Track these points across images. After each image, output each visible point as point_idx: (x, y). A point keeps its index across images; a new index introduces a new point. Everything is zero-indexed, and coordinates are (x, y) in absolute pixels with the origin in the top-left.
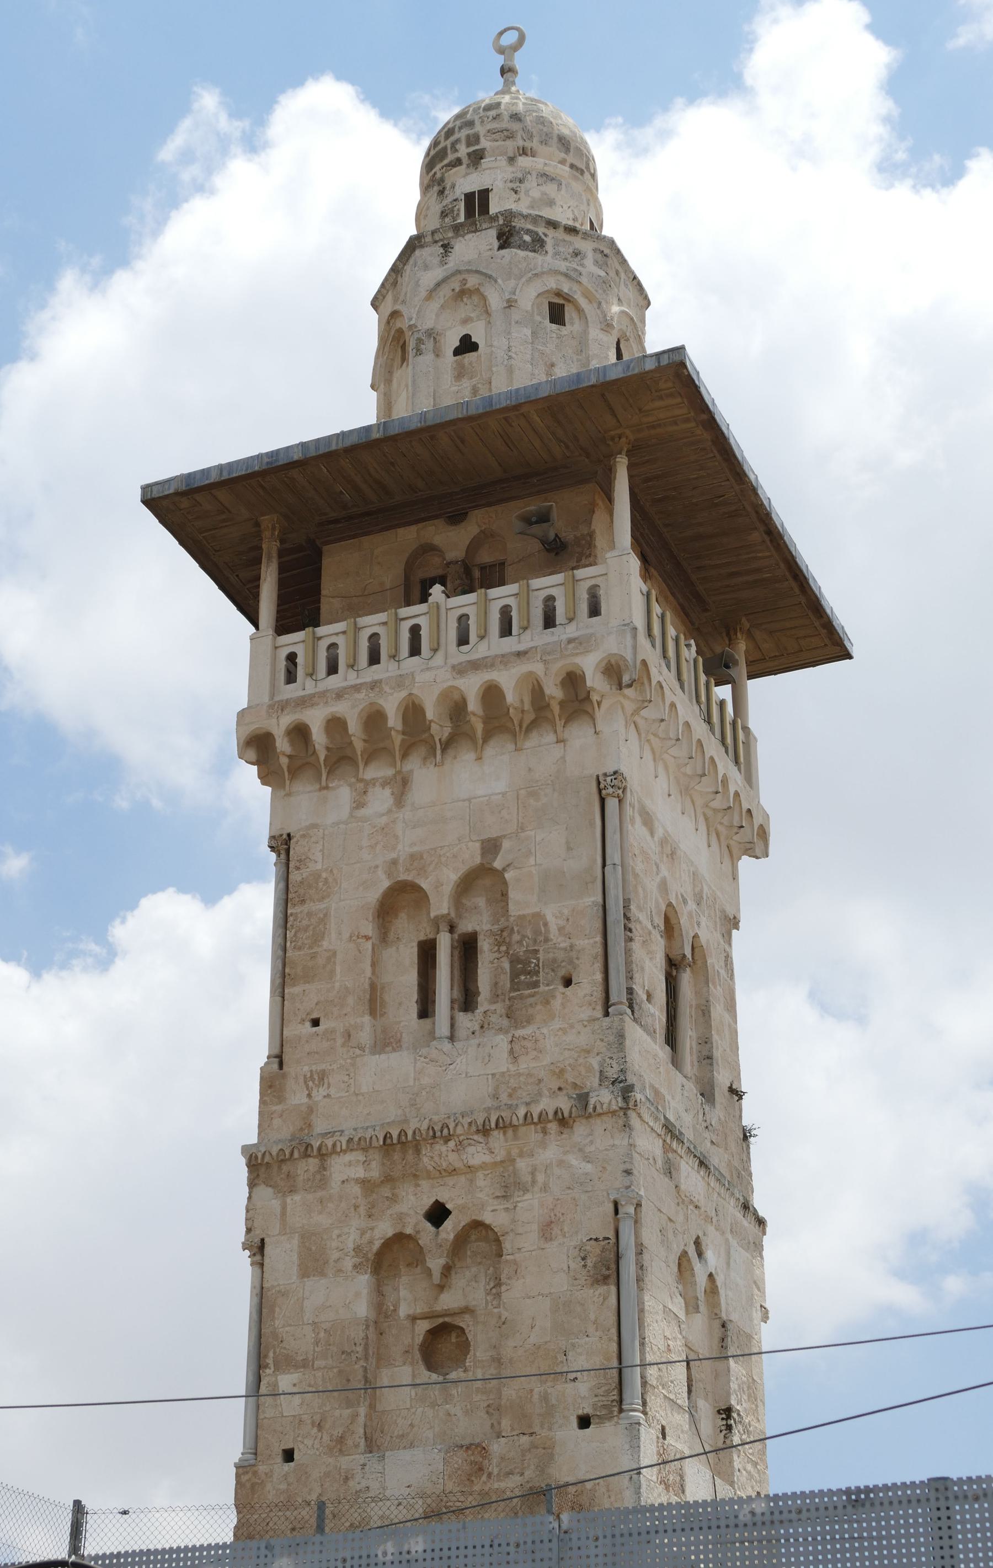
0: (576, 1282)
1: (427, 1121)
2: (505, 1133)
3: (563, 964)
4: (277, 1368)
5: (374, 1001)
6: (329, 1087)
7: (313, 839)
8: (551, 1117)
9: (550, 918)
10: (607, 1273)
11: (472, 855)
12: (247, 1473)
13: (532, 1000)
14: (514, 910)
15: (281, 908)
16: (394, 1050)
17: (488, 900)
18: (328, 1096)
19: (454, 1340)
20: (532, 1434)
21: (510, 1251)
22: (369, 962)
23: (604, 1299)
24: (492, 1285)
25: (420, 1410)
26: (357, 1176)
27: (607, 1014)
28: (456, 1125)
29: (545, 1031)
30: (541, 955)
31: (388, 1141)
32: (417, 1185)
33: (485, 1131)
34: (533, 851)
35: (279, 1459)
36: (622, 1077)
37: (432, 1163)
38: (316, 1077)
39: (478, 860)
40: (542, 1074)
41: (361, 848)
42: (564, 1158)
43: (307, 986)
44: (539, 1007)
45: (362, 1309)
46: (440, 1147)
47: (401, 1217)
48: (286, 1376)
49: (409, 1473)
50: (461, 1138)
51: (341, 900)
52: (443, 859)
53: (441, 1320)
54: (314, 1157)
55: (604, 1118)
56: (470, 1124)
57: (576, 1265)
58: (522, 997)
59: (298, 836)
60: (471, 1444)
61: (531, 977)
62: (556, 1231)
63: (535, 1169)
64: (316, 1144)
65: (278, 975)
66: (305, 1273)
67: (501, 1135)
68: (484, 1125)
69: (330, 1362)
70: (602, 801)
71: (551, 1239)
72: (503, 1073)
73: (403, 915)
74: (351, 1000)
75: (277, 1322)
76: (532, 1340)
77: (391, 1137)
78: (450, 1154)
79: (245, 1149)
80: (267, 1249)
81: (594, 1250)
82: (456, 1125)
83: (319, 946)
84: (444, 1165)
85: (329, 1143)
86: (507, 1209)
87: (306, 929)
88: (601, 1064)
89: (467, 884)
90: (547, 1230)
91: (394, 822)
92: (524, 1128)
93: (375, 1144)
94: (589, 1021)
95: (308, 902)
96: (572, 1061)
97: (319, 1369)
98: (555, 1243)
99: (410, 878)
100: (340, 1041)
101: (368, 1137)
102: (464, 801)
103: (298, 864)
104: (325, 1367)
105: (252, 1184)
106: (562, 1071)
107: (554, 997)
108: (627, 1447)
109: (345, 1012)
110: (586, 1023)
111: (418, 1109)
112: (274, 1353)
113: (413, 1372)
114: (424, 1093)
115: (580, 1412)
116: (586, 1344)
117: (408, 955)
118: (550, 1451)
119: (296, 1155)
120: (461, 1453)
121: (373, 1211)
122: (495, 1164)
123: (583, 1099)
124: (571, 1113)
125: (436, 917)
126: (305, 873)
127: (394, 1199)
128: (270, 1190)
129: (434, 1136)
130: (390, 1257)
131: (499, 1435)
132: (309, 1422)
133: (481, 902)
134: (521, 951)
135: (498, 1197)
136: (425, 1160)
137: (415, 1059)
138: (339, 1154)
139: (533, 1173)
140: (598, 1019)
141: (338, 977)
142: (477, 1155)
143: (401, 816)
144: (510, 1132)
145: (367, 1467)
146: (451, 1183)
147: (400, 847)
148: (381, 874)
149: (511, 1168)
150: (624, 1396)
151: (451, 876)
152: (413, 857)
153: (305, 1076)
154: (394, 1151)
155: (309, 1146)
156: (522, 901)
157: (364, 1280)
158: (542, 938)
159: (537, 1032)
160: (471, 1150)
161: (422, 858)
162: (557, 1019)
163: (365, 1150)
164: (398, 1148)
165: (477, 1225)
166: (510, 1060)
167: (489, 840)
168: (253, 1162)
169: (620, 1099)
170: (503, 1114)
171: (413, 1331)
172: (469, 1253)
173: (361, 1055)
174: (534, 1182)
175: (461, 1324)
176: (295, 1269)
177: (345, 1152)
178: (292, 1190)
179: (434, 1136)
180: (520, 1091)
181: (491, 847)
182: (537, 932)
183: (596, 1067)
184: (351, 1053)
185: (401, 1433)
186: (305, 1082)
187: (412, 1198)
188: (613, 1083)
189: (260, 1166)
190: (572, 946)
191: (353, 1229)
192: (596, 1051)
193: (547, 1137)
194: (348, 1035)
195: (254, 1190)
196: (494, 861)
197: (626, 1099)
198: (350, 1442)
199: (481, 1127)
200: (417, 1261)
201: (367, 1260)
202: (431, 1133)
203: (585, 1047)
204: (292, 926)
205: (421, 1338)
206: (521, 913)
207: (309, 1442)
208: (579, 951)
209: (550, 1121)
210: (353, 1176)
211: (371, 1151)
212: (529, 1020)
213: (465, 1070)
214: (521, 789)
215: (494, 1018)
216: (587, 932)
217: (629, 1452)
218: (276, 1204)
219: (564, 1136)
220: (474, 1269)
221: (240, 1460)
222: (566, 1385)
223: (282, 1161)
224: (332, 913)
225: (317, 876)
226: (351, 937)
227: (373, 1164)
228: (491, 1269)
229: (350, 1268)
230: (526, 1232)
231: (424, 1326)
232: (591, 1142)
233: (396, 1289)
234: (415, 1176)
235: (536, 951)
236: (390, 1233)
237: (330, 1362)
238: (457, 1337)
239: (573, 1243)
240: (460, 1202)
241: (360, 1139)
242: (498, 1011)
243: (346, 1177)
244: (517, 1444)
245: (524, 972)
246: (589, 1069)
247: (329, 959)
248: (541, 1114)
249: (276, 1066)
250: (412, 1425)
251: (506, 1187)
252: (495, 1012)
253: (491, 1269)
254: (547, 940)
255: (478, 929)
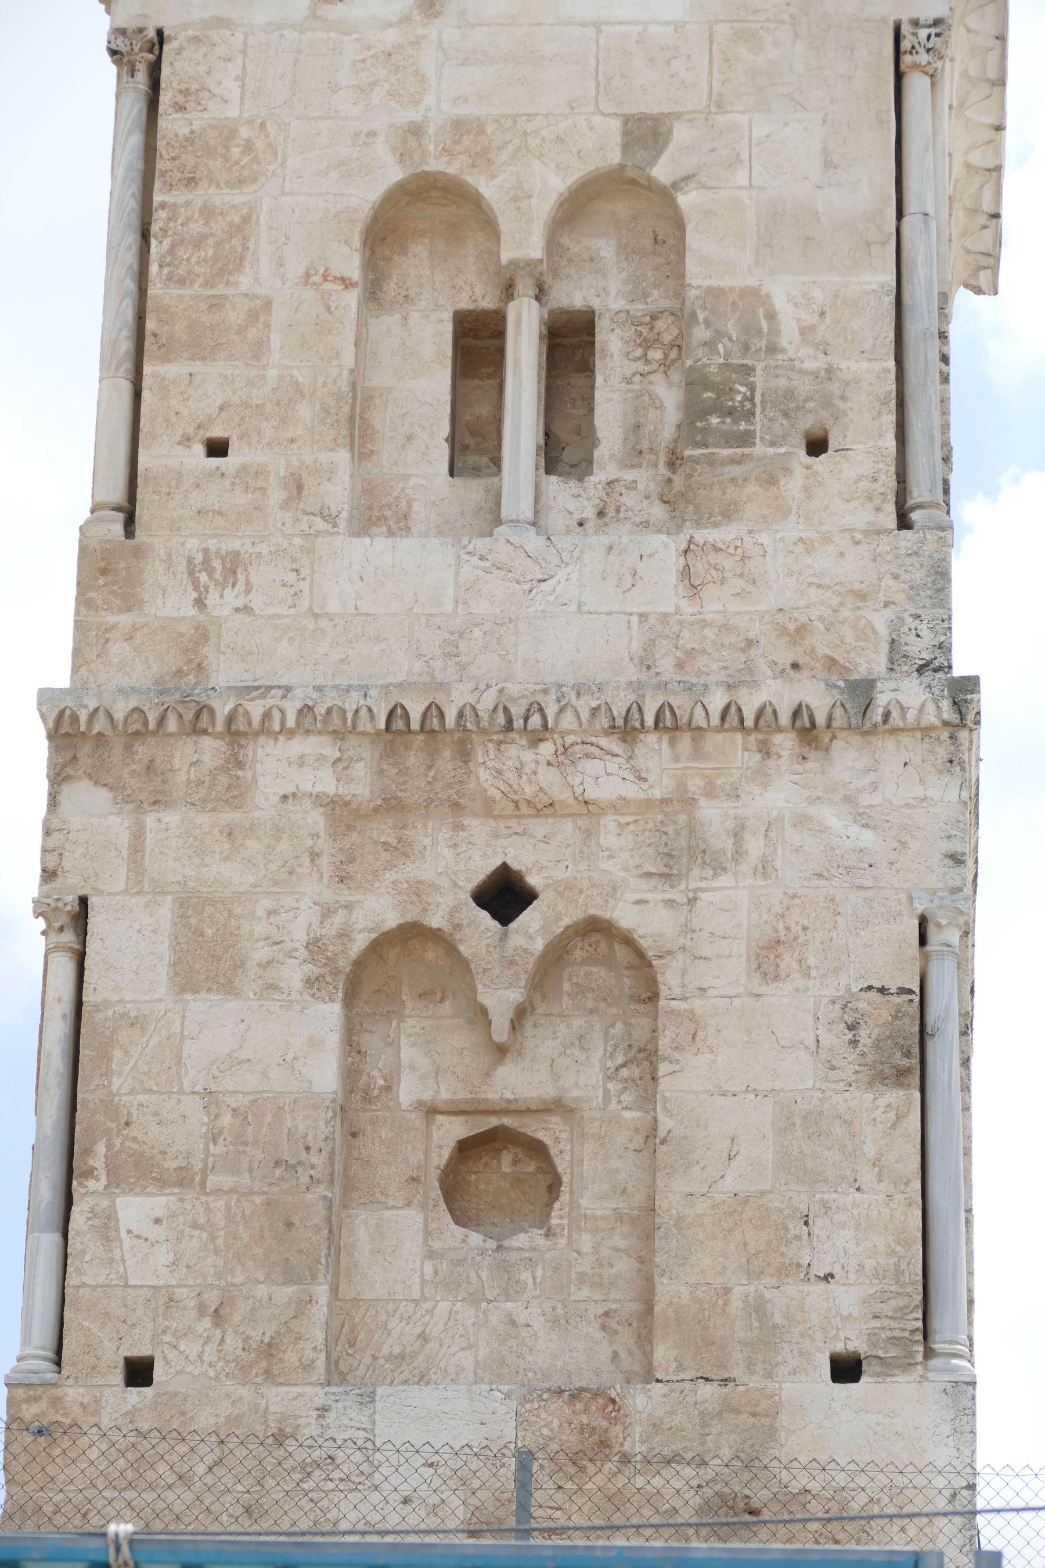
0: (832, 1074)
1: (493, 692)
2: (672, 742)
3: (810, 405)
4: (116, 1179)
5: (357, 422)
6: (248, 592)
7: (219, 51)
8: (785, 719)
9: (780, 303)
10: (906, 1062)
11: (602, 146)
12: (37, 1399)
13: (736, 470)
14: (697, 275)
15: (135, 188)
16: (391, 534)
17: (623, 250)
18: (246, 609)
19: (506, 1168)
20: (725, 1382)
21: (677, 992)
22: (351, 336)
23: (898, 1118)
24: (620, 1059)
25: (443, 1306)
26: (319, 788)
27: (904, 522)
28: (561, 710)
29: (764, 538)
30: (758, 379)
31: (399, 724)
32: (458, 827)
33: (627, 730)
34: (745, 155)
35: (118, 1376)
36: (941, 660)
37: (501, 785)
38: (217, 564)
39: (615, 157)
40: (756, 630)
41: (335, 89)
42: (812, 810)
43: (198, 367)
44: (753, 488)
45: (325, 1075)
46: (518, 752)
47: (418, 890)
48: (138, 1200)
49: (430, 1437)
50: (570, 739)
51: (283, 193)
52: (533, 142)
53: (493, 1122)
54: (217, 736)
55: (905, 739)
56: (595, 711)
57: (834, 1038)
58: (712, 462)
59: (182, 37)
60: (581, 1390)
61: (736, 422)
62: (788, 961)
63: (743, 827)
64: (223, 708)
65: (126, 333)
66: (186, 981)
67: (665, 745)
68: (626, 719)
69: (246, 1180)
70: (899, 76)
71: (777, 978)
72: (666, 615)
73: (419, 250)
74: (305, 412)
75: (116, 1082)
76: (730, 1183)
77: (441, 715)
78: (542, 769)
79: (46, 696)
80: (96, 922)
81: (878, 1014)
82: (561, 710)
83: (228, 284)
84: (529, 791)
85: (256, 710)
86: (670, 903)
87: (198, 243)
88: (895, 625)
89: (576, 208)
90: (768, 957)
91: (416, 43)
92: (720, 737)
93: (365, 724)
94: (866, 533)
95: (204, 183)
96: (826, 612)
97: (218, 1192)
98: (787, 987)
99: (452, 170)
100: (276, 496)
101: (350, 707)
102: (584, 25)
103: (180, 99)
104: (233, 1191)
105: (59, 777)
106: (802, 630)
107: (788, 471)
108: (946, 1429)
109: (289, 435)
110: (859, 536)
111: (463, 667)
112: (109, 1146)
113: (426, 1224)
114: (477, 633)
115: (839, 1347)
116: (855, 1205)
117: (435, 339)
118: (767, 1421)
119: (172, 725)
120: (557, 1404)
121: (352, 869)
122: (648, 804)
123: (862, 692)
124: (830, 719)
125: (514, 263)
126: (199, 121)
127: (401, 850)
128: (103, 795)
129: (509, 726)
130: (387, 972)
131: (649, 1375)
132: (193, 1303)
133: (606, 249)
134: (713, 363)
135: (649, 875)
136: (484, 775)
137: (459, 557)
138: (275, 736)
139: (737, 834)
140: (888, 532)
141: (275, 356)
142: (605, 778)
143: (434, 36)
144: (685, 742)
145: (331, 1415)
146: (540, 833)
147: (429, 100)
148: (381, 149)
149: (682, 818)
150: (936, 1324)
151: (551, 183)
152: (459, 126)
153: (190, 561)
154: (408, 747)
155: (203, 710)
156: (715, 258)
157: (329, 1014)
158: (763, 344)
159: (747, 538)
160: (592, 767)
161: (481, 130)
162: (793, 518)
163: (338, 735)
164: (420, 741)
165: (595, 928)
166: (681, 590)
167: (641, 119)
168: (65, 728)
169: (945, 704)
170: (675, 702)
171: (428, 1136)
172: (566, 986)
173: (327, 533)
174: (739, 853)
175: (540, 1135)
176: (163, 973)
177: (291, 733)
178: (157, 803)
179: (509, 726)
180: (701, 661)
181: (646, 133)
182: (750, 330)
183: (884, 632)
184: (304, 526)
185: (397, 1351)
186: (191, 573)
187: (447, 853)
188: (921, 670)
189: (76, 739)
190: (830, 371)
191: (305, 903)
192: (882, 598)
193: (771, 763)
194: (297, 486)
195: (66, 789)
196: (654, 160)
197: (957, 705)
198: (291, 1357)
199: (620, 722)
200: (444, 990)
201: (336, 972)
202: (501, 719)
203: (857, 586)
204: (164, 231)
205: (446, 1154)
206: (714, 283)
207: (191, 1347)
208: (847, 384)
209: (780, 730)
210: (308, 787)
211: (353, 740)
212: (729, 513)
213: (574, 595)
214: (718, 22)
215: (629, 500)
216: (867, 346)
217: (950, 1442)
218: (118, 826)
219: (809, 765)
220: (578, 1022)
221: (14, 1370)
222: (807, 1288)
223: (137, 733)
224: (263, 218)
225: (228, 132)
226: (307, 275)
227: (360, 769)
228: (619, 1025)
229: (297, 985)
230: (719, 956)
231: (452, 1131)
232: (875, 787)
233: (392, 1044)
234: (456, 806)
235: (748, 370)
236: (392, 921)
237: (246, 1180)
238: (515, 1162)
239: (830, 992)
240: (560, 874)
241: (329, 711)
242: (641, 486)
243: (290, 789)
244: (691, 1399)
245: (716, 410)
246: (865, 633)
247: (253, 316)
248: (760, 714)
249: (118, 529)
250: (423, 1337)
251: (670, 855)
252: (632, 486)
253: (619, 1025)
254: (772, 349)
255: (596, 304)
